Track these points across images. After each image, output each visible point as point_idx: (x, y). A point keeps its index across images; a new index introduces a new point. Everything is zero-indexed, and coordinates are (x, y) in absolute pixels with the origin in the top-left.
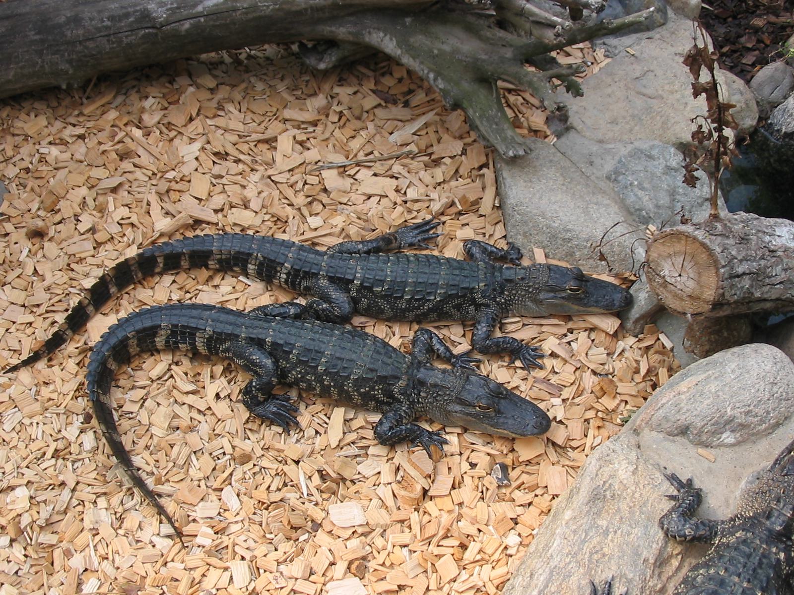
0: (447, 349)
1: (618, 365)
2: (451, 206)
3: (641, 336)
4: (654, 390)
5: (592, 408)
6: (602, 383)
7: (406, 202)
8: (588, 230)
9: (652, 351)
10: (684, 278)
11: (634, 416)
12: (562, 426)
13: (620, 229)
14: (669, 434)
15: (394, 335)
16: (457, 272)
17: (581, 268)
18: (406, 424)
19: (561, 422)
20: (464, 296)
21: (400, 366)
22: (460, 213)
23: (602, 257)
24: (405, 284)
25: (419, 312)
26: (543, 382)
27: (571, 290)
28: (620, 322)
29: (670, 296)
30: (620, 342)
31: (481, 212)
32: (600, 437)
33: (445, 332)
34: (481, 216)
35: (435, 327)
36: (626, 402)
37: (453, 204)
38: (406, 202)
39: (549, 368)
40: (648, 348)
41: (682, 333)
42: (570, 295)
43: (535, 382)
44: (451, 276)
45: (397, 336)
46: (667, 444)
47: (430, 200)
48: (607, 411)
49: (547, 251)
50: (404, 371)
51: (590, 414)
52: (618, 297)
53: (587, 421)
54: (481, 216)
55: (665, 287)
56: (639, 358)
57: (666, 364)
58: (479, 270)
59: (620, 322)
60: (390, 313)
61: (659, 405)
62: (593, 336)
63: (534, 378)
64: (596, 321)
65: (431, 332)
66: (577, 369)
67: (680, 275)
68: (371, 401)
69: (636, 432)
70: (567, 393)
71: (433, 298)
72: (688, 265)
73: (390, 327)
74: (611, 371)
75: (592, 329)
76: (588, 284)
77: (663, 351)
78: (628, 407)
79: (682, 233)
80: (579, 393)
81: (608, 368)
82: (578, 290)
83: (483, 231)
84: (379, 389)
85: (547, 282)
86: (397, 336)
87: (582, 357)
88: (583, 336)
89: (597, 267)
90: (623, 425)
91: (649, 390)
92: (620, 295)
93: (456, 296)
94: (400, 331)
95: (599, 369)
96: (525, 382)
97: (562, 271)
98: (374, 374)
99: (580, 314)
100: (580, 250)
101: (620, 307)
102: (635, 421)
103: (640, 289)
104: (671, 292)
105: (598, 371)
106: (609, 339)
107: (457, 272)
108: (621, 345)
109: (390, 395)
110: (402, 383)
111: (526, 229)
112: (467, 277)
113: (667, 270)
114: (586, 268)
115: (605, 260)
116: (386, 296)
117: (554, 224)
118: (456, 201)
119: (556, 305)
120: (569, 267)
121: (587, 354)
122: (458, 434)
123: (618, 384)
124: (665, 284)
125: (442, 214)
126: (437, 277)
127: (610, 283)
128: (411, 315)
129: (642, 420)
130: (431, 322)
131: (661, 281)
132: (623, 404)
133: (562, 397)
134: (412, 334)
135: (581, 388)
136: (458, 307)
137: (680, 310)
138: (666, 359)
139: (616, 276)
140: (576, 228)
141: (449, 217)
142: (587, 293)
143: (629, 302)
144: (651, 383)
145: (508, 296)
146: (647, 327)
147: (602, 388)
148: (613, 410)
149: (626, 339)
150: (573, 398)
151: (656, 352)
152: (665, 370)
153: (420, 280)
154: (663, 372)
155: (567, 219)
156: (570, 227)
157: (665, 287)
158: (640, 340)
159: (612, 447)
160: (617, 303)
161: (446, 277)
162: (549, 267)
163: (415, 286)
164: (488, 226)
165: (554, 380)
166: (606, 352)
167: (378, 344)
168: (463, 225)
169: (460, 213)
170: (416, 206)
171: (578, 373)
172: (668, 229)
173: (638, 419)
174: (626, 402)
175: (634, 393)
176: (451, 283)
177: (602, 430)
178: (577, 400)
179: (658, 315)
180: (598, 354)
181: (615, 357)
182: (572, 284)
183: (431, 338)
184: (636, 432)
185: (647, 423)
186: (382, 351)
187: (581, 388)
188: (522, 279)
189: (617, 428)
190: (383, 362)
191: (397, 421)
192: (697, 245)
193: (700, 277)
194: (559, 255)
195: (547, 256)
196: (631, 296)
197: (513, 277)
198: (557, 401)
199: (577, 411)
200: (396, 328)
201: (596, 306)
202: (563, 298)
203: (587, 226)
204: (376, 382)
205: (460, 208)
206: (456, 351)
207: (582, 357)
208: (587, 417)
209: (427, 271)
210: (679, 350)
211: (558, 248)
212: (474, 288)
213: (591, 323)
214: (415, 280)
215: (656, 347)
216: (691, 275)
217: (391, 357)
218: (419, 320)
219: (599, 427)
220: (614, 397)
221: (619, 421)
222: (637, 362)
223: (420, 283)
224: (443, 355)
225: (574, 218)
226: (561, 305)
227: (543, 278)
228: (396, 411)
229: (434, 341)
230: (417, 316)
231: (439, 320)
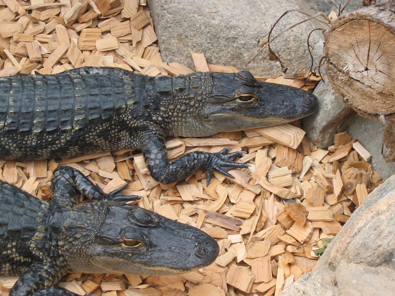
0: (96, 188)
1: (306, 186)
2: (87, 11)
3: (331, 148)
4: (352, 212)
5: (280, 241)
6: (288, 211)
7: (30, 11)
8: (257, 24)
9: (346, 165)
10: (372, 72)
11: (329, 245)
12: (244, 268)
13: (293, 19)
14: (371, 264)
15: (28, 177)
16: (96, 91)
17: (252, 72)
18: (49, 287)
19: (242, 263)
20: (109, 119)
21: (35, 215)
22: (98, 19)
23: (273, 56)
24: (32, 115)
25: (55, 147)
26: (217, 216)
27: (241, 98)
28: (304, 133)
29: (357, 96)
30: (307, 158)
31: (125, 15)
32: (292, 277)
33: (92, 167)
34: (125, 19)
35: (79, 163)
36: (320, 230)
37: (89, 8)
38: (30, 11)
39: (223, 199)
40: (341, 162)
41: (380, 139)
42: (240, 106)
43: (207, 217)
44: (90, 98)
45: (33, 178)
46: (368, 277)
47: (60, 6)
48: (299, 244)
49: (208, 55)
50: (39, 220)
51: (278, 250)
52: (300, 104)
53: (275, 258)
54: (125, 19)
55: (351, 85)
56: (331, 175)
57: (364, 177)
58: (124, 84)
59: (304, 133)
60: (17, 153)
61: (356, 230)
62: (273, 153)
63: (206, 212)
64: (274, 134)
65: (73, 170)
66: (257, 196)
67: (367, 69)
68: (5, 263)
69: (332, 266)
70: (247, 227)
71: (69, 128)
72: (375, 55)
73: (23, 169)
74: (299, 194)
75: (272, 146)
76: (262, 90)
77: (359, 163)
78: (323, 236)
79: (363, 17)
80: (262, 225)
81: (295, 190)
82: (250, 98)
83: (129, 38)
84: (13, 247)
85: (211, 93)
86: (33, 178)
87: (262, 182)
88: (261, 155)
89: (271, 69)
90: (317, 259)
91: (347, 212)
92: (302, 99)
93: (100, 121)
94: (36, 172)
95: (284, 194)
96: (194, 218)
97: (227, 77)
98: (4, 228)
99: (255, 128)
100: (248, 50)
101: (304, 113)
102: (329, 252)
103: (324, 91)
104: (357, 90)
105: (283, 196)
106: (293, 155)
107: (96, 91)
108: (308, 161)
109: (28, 254)
110: (38, 235)
111: (181, 31)
112: (110, 95)
113: (351, 64)
114: (259, 71)
115: (277, 59)
116: (9, 132)
117: (214, 22)
118: (93, 4)
119: (225, 120)
120: (237, 71)
121: (267, 177)
122: (118, 292)
123: (308, 209)
124: (350, 81)
125: (77, 21)
126: (71, 101)
127: (287, 87)
128: (45, 153)
129: (337, 251)
130: (72, 157)
131: (345, 78)
132: (317, 233)
133: (242, 232)
134: (50, 173)
135: (264, 219)
136: (104, 134)
137: (370, 111)
138: (364, 172)
139: (296, 77)
140: (241, 24)
141: (85, 25)
142: (261, 100)
143: (314, 107)
144: (349, 204)
145: (165, 112)
146: (337, 136)
147: (289, 217)
148: (305, 242)
149: (313, 154)
150: (255, 232)
151: (351, 166)
152: (363, 186)
153: (51, 108)
154: (361, 189)
155: (229, 14)
156: (234, 22)
157: (351, 85)
158: (331, 153)
159: (302, 288)
160: (299, 110)
161: (83, 99)
162: (212, 75)
163: (45, 116)
164: (135, 32)
165: (231, 212)
166: (291, 172)
167: (7, 192)
168: (103, 33)
169: (98, 19)
170: (44, 15)
171: (258, 200)
172: (346, 14)
173: (332, 251)
174: (320, 230)
175: (328, 218)
176: (90, 106)
177: (294, 268)
178: (260, 235)
179: (348, 121)
180: (281, 175)
181: (302, 176)
182: (242, 92)
183: (74, 177)
184: (332, 266)
185: (343, 254)
186: (12, 199)
187: (264, 219)
188: (181, 90)
189: (311, 263)
190: (15, 214)
191: (37, 284)
192: (384, 30)
193: (390, 69)
194: (224, 59)
195: (209, 61)
196: (316, 98)
197: (169, 89)
198: (236, 238)
199: (261, 248)
200: (31, 170)
201: (275, 115)
202: (233, 109)
203: (255, 20)
204: (7, 239)
205: (98, 12)
206: (107, 189)
207: (262, 182)
208: (273, 253)
209: (58, 96)
210: (379, 160)
211: (221, 50)
212: (120, 108)
213: (269, 138)
214: (44, 108)
215: (352, 159)
216: (380, 68)
217: (23, 206)
218: (58, 155)
219: (290, 265)
220: (305, 226)
221: (313, 254)
222: (329, 180)
223: (51, 111)
224: (91, 196)
225: (238, 11)
226: (232, 119)
227: (206, 88)
228: (35, 272)
229: (79, 179)
230: (53, 152)
231: (83, 154)
